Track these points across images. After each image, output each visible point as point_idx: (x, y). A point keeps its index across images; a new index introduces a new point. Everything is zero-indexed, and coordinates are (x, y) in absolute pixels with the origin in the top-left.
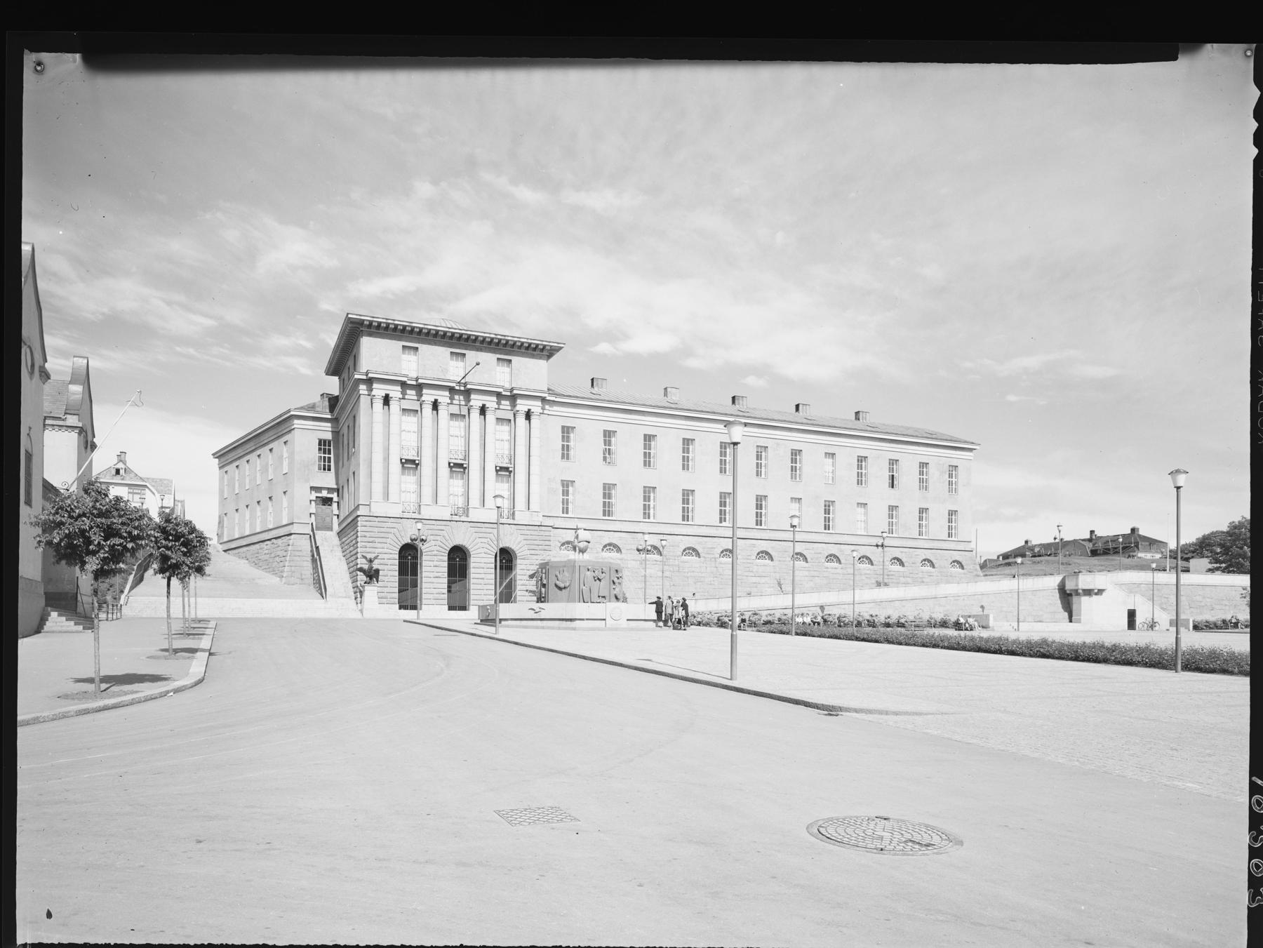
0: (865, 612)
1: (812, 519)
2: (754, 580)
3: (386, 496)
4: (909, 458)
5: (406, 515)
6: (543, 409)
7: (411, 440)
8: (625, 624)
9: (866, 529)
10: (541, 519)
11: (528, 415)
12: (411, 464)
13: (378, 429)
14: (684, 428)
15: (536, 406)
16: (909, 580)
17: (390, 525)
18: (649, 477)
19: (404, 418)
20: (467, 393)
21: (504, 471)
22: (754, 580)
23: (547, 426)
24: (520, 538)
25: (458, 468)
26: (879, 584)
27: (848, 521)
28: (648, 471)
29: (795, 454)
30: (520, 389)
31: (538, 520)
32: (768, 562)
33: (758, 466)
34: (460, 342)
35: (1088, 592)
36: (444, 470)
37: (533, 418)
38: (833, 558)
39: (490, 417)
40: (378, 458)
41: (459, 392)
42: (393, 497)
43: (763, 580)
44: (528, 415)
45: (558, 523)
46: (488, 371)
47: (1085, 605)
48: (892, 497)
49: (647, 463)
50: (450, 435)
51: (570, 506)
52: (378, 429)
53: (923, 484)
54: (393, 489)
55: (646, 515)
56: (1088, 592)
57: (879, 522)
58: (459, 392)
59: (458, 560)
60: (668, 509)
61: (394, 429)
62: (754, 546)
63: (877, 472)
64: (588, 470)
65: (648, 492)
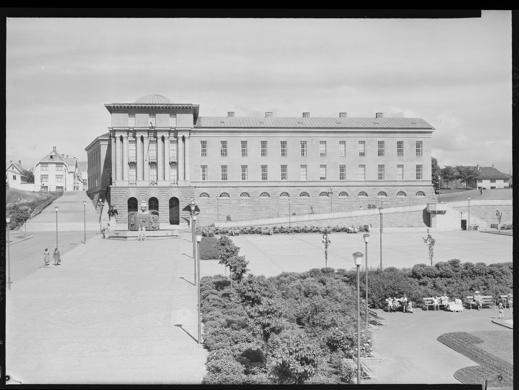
1: (333, 175)
2: (297, 206)
4: (391, 142)
5: (130, 186)
6: (190, 135)
7: (153, 154)
11: (184, 138)
12: (132, 164)
13: (119, 150)
14: (263, 137)
15: (186, 135)
16: (389, 203)
17: (123, 190)
19: (130, 145)
20: (156, 132)
21: (174, 164)
22: (297, 206)
26: (370, 207)
27: (354, 174)
28: (264, 158)
29: (284, 144)
30: (178, 128)
31: (188, 184)
33: (303, 151)
34: (152, 110)
35: (440, 212)
37: (187, 141)
38: (304, 194)
39: (166, 141)
41: (151, 131)
42: (126, 178)
43: (303, 206)
44: (184, 138)
46: (165, 121)
49: (283, 154)
50: (151, 151)
51: (206, 177)
52: (119, 150)
54: (125, 175)
56: (440, 212)
57: (373, 174)
58: (151, 131)
59: (153, 203)
60: (254, 175)
61: (125, 150)
62: (299, 190)
63: (372, 148)
64: (214, 159)
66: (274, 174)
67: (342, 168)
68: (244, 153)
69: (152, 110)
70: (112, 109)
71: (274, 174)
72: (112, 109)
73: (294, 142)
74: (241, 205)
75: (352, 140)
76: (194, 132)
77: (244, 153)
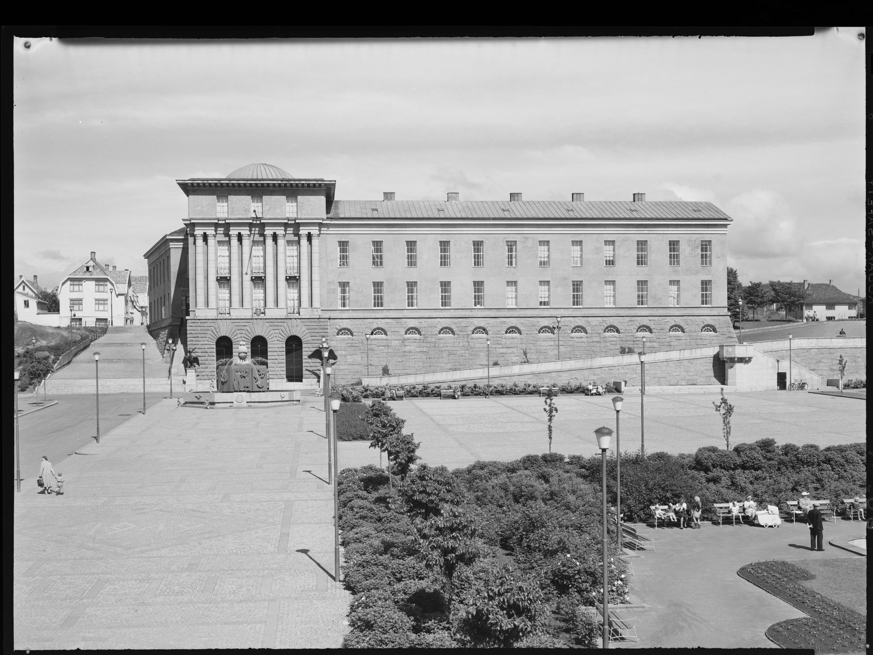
0: (495, 383)
1: (562, 297)
3: (207, 304)
5: (220, 317)
8: (245, 405)
9: (614, 303)
10: (320, 312)
12: (224, 281)
15: (314, 231)
16: (655, 344)
18: (378, 275)
19: (219, 248)
20: (262, 226)
21: (293, 280)
22: (501, 351)
23: (326, 244)
24: (304, 328)
25: (259, 281)
26: (623, 351)
27: (597, 296)
28: (444, 269)
30: (300, 219)
31: (317, 314)
32: (517, 335)
33: (510, 257)
34: (257, 189)
35: (742, 360)
36: (248, 283)
38: (512, 329)
40: (200, 278)
41: (256, 225)
43: (510, 351)
44: (309, 237)
45: (406, 314)
46: (280, 208)
47: (736, 373)
48: (642, 273)
50: (255, 257)
51: (347, 301)
52: (200, 258)
53: (674, 258)
55: (411, 304)
56: (742, 360)
57: (628, 295)
58: (256, 225)
59: (259, 346)
61: (211, 256)
62: (504, 322)
65: (411, 285)
66: (462, 294)
67: (577, 286)
68: (412, 262)
69: (257, 189)
70: (190, 188)
71: (462, 294)
72: (190, 188)
73: (495, 241)
74: (407, 349)
75: (593, 238)
76: (327, 226)
77: (412, 262)
